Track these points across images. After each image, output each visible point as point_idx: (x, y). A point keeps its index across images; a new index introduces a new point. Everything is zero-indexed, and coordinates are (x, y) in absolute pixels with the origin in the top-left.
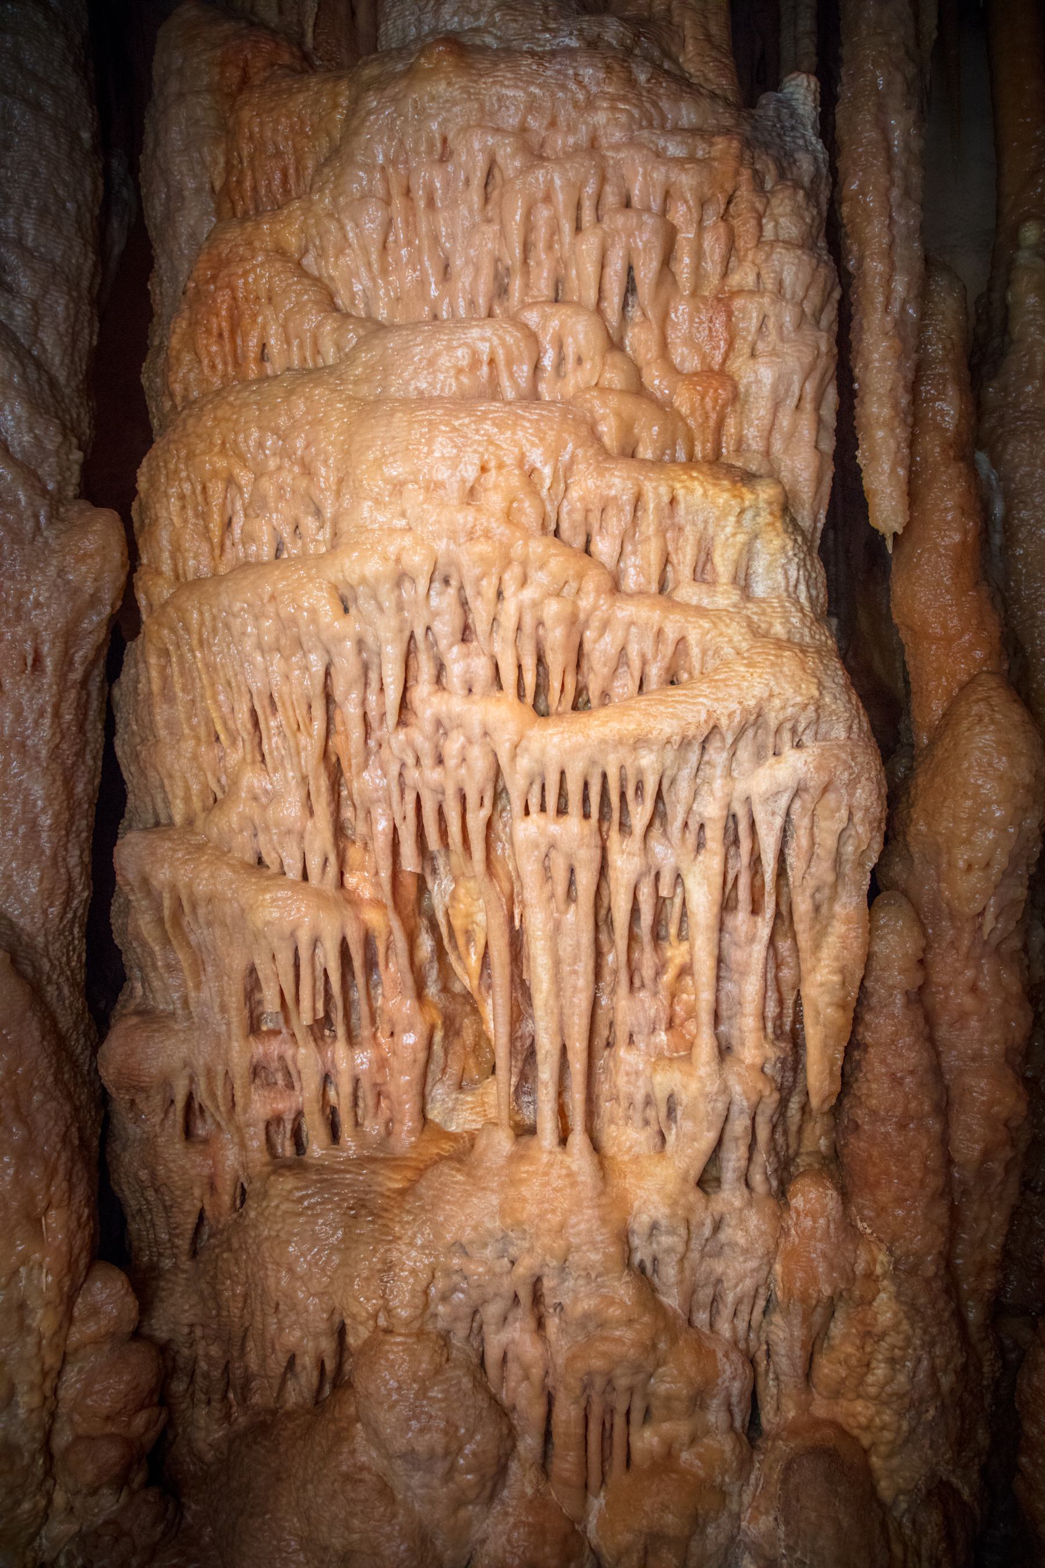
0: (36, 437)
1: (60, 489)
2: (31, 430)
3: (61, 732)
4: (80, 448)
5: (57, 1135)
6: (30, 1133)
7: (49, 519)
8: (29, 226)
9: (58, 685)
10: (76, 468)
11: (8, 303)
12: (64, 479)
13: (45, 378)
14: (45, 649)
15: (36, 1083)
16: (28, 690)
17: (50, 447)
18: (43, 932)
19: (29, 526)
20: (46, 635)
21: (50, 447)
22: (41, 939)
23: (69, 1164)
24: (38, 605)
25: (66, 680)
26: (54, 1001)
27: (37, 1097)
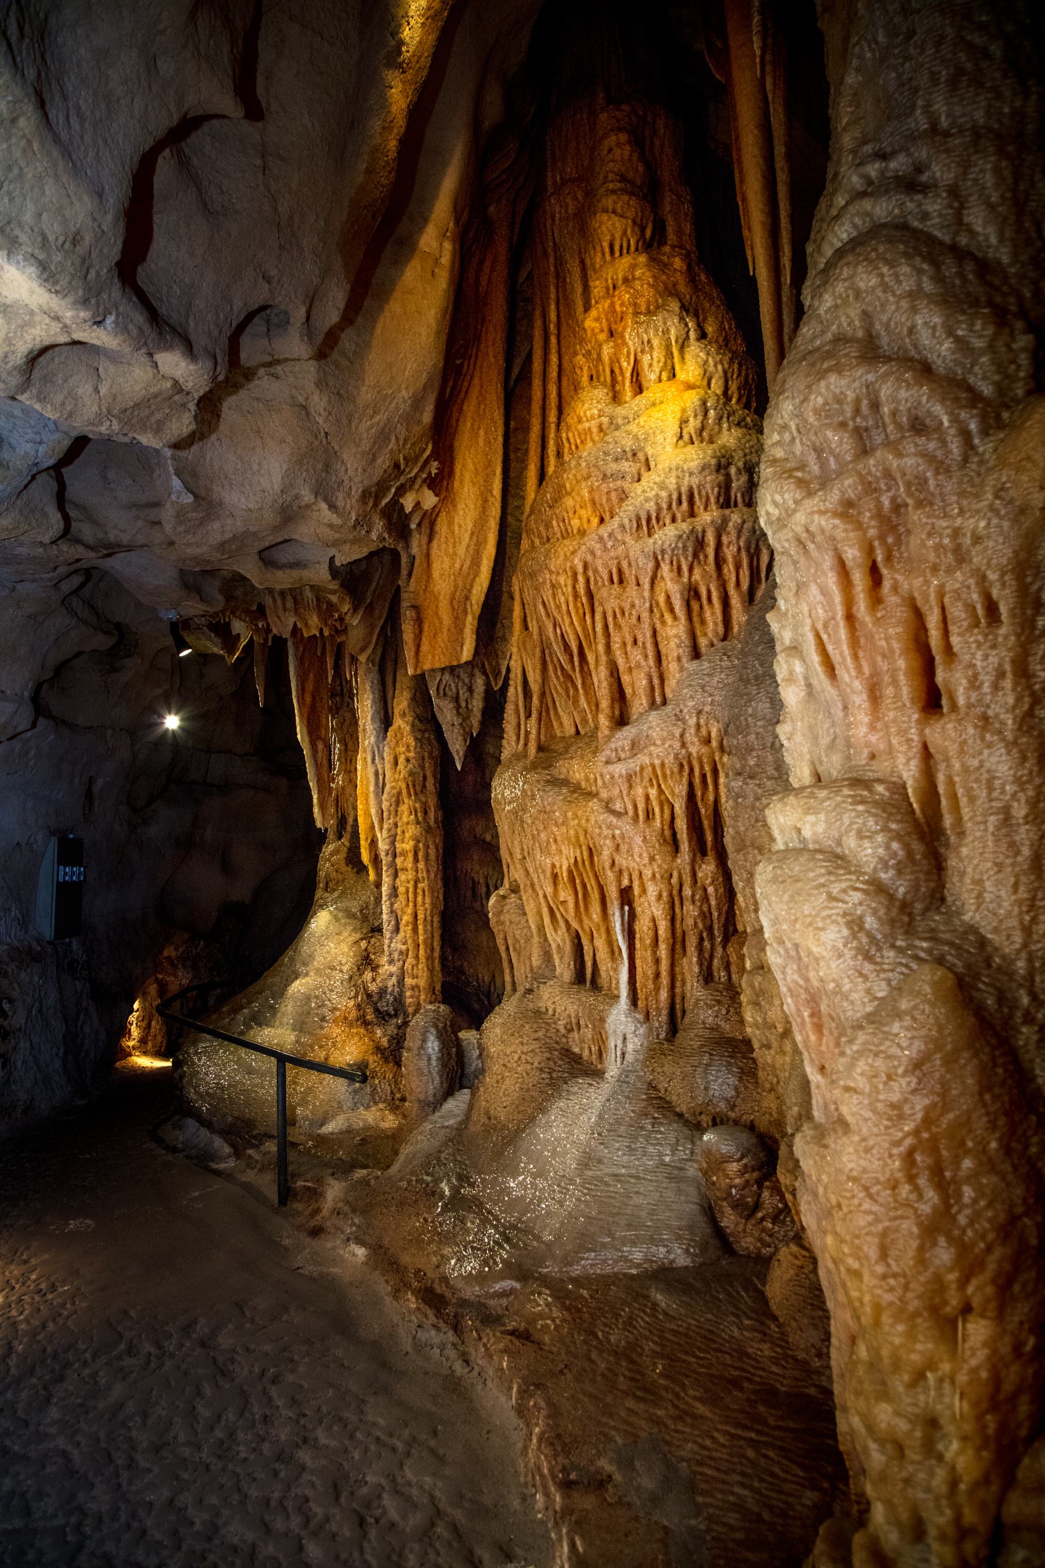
0: (958, 340)
1: (1001, 390)
2: (950, 333)
3: (1033, 694)
4: (1027, 331)
5: (990, 1220)
6: (948, 1207)
7: (985, 432)
8: (940, 106)
9: (1018, 636)
10: (1024, 359)
11: (920, 205)
12: (1007, 376)
13: (969, 267)
14: (995, 593)
15: (970, 1144)
16: (979, 647)
17: (979, 344)
18: (1024, 955)
19: (955, 447)
20: (992, 576)
21: (979, 344)
22: (1021, 964)
23: (1007, 1266)
24: (977, 539)
25: (1033, 627)
26: (1032, 1047)
27: (967, 1163)
